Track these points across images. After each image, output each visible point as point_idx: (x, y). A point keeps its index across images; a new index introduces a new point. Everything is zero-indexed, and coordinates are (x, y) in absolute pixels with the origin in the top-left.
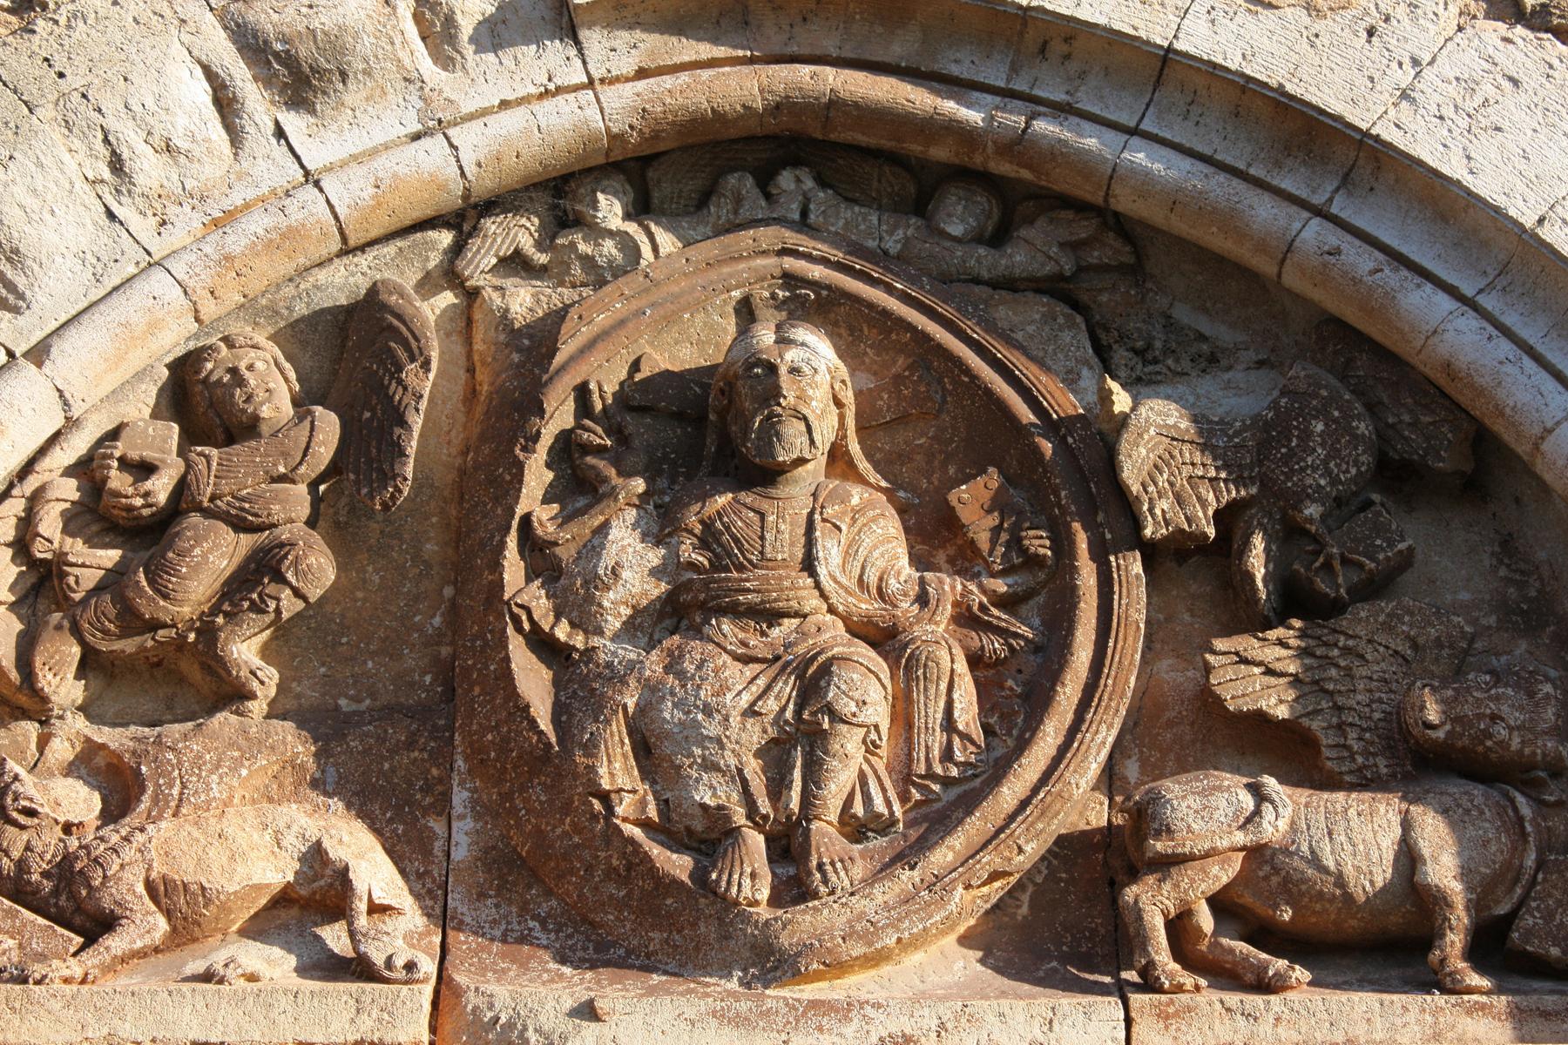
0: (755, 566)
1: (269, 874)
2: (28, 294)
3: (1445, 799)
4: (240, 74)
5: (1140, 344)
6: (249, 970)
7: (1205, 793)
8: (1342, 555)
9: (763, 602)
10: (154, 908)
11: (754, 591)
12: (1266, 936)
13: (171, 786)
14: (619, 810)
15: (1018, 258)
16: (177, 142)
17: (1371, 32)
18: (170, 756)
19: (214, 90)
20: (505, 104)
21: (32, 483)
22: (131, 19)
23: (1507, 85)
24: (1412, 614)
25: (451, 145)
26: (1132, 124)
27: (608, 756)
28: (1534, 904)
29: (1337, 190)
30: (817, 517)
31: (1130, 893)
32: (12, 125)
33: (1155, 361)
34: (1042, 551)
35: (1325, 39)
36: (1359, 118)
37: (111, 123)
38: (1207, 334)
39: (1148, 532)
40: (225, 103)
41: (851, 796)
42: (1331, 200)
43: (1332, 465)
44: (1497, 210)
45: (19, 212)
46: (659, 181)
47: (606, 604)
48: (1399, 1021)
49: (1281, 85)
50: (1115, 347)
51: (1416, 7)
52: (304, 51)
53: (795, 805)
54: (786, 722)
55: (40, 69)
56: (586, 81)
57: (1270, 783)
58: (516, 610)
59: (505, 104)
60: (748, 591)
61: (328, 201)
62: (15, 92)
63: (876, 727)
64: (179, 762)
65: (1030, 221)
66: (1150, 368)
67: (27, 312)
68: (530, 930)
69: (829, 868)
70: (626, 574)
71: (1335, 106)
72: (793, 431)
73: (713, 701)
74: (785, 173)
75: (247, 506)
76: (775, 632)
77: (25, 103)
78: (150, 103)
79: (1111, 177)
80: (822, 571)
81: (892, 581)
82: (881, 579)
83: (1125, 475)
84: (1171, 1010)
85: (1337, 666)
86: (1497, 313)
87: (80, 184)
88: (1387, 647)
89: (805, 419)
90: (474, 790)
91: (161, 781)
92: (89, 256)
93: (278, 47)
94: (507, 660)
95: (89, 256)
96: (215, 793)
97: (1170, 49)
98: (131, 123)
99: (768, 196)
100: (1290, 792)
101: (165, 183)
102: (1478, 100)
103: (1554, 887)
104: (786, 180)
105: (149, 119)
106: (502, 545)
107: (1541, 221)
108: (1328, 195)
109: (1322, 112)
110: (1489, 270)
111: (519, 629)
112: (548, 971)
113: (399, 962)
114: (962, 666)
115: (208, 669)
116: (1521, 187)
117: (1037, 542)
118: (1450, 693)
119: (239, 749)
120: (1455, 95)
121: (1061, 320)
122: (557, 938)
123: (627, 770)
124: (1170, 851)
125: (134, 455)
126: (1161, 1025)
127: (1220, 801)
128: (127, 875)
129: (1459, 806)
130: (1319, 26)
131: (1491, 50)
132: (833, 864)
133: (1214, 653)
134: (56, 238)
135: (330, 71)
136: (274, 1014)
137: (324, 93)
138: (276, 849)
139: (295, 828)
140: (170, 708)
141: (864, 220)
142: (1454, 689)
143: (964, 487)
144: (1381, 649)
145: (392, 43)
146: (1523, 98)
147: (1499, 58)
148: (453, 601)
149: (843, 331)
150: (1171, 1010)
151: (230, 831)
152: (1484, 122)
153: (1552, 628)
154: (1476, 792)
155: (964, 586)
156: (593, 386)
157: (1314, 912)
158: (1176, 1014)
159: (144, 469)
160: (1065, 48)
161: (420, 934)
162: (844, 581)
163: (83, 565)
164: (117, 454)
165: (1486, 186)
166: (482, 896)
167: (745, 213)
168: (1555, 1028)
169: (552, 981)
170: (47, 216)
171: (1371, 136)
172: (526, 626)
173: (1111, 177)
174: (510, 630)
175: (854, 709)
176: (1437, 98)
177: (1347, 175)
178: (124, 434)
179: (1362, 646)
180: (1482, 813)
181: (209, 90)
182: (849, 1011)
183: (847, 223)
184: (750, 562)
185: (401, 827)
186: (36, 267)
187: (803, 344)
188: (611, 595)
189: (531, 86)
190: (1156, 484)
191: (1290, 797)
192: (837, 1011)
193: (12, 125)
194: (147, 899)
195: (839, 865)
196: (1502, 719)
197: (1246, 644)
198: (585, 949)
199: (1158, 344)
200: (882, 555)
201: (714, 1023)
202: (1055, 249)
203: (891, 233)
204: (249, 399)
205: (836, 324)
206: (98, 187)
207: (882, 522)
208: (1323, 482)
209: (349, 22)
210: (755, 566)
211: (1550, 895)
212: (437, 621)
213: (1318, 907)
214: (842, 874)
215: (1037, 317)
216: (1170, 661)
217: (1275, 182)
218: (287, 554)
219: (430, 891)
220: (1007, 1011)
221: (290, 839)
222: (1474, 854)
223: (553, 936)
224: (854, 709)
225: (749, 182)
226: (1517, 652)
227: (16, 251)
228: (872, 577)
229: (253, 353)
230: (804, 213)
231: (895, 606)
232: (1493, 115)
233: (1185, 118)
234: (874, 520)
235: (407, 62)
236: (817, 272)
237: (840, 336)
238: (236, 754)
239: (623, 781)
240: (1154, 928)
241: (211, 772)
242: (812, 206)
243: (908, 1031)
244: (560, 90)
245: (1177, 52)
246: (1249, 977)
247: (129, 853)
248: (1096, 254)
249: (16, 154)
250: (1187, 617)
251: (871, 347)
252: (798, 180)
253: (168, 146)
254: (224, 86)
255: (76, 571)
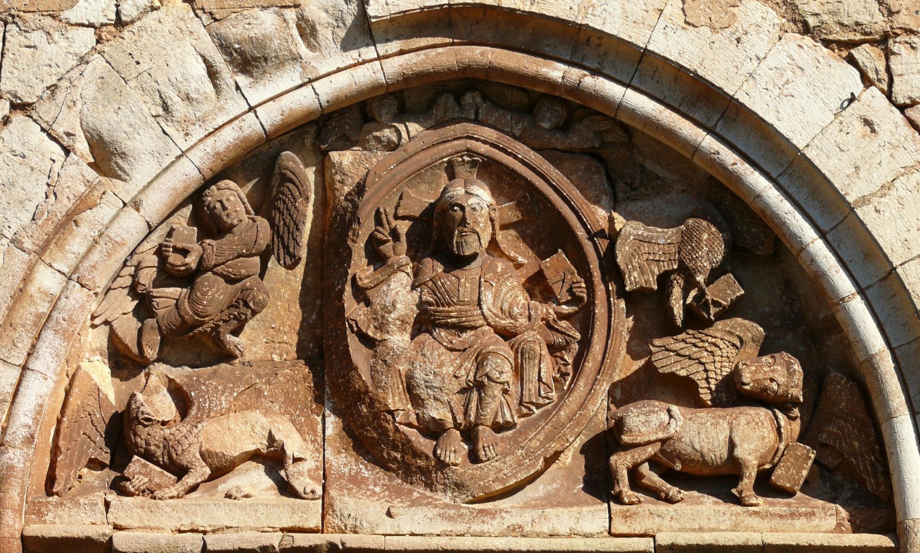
0: (455, 304)
1: (250, 446)
2: (130, 173)
3: (749, 417)
4: (219, 60)
5: (629, 181)
6: (246, 493)
7: (647, 414)
8: (713, 300)
9: (458, 323)
10: (204, 464)
11: (455, 317)
12: (669, 475)
13: (205, 403)
14: (397, 419)
15: (574, 140)
16: (193, 95)
17: (738, 40)
18: (203, 388)
19: (207, 67)
20: (339, 70)
21: (136, 258)
22: (168, 32)
23: (798, 71)
24: (741, 327)
25: (316, 93)
26: (628, 82)
27: (393, 394)
28: (782, 464)
29: (719, 120)
30: (482, 280)
31: (613, 459)
32: (118, 91)
33: (636, 189)
34: (581, 294)
35: (716, 45)
36: (730, 90)
37: (163, 89)
38: (660, 175)
39: (627, 289)
40: (213, 74)
41: (497, 413)
42: (716, 125)
43: (710, 255)
44: (788, 140)
45: (124, 135)
46: (409, 96)
47: (390, 320)
48: (721, 519)
49: (696, 71)
50: (618, 180)
51: (760, 27)
52: (247, 48)
53: (472, 418)
54: (469, 381)
55: (128, 60)
56: (376, 56)
57: (675, 409)
58: (351, 322)
59: (339, 70)
60: (452, 317)
61: (261, 123)
62: (118, 72)
63: (508, 383)
64: (208, 391)
65: (581, 120)
66: (633, 193)
67: (130, 182)
68: (361, 469)
69: (487, 449)
70: (398, 306)
71: (719, 82)
72: (472, 238)
73: (437, 370)
74: (468, 95)
75: (231, 270)
76: (464, 335)
77: (123, 78)
78: (179, 77)
79: (617, 109)
80: (485, 307)
81: (515, 309)
82: (510, 308)
83: (618, 260)
84: (628, 514)
85: (707, 350)
86: (786, 187)
87: (151, 119)
88: (729, 342)
89: (478, 234)
90: (334, 403)
91: (201, 400)
92: (156, 153)
93: (237, 46)
94: (347, 346)
95: (156, 153)
96: (224, 405)
97: (645, 49)
98: (171, 88)
99: (459, 104)
100: (683, 411)
101: (187, 115)
102: (785, 80)
103: (791, 457)
104: (468, 98)
105: (180, 85)
106: (342, 291)
107: (807, 146)
108: (715, 122)
109: (713, 85)
110: (784, 164)
111: (353, 331)
112: (369, 490)
113: (308, 490)
114: (545, 352)
115: (215, 343)
116: (800, 128)
117: (579, 290)
118: (754, 368)
119: (232, 383)
120: (773, 76)
121: (593, 169)
122: (372, 474)
123: (400, 400)
124: (631, 442)
125: (179, 245)
126: (624, 521)
127: (653, 417)
128: (192, 449)
129: (753, 421)
130: (715, 37)
131: (792, 53)
132: (488, 447)
133: (653, 346)
134: (141, 146)
135: (260, 58)
136: (259, 514)
137: (257, 67)
138: (252, 434)
139: (259, 423)
140: (199, 358)
141: (504, 118)
142: (756, 366)
143: (548, 260)
144: (727, 343)
145: (288, 42)
146: (804, 80)
147: (796, 57)
148: (321, 307)
149: (494, 177)
150: (628, 514)
151: (232, 426)
152: (786, 92)
153: (803, 327)
154: (761, 413)
155: (547, 310)
156: (382, 210)
157: (691, 467)
158: (630, 516)
159: (185, 252)
160: (598, 41)
161: (314, 470)
162: (495, 311)
163: (160, 297)
164: (172, 245)
165: (782, 127)
166: (339, 452)
167: (449, 115)
168: (785, 522)
169: (371, 496)
170: (137, 136)
171: (734, 99)
172: (355, 329)
173: (617, 109)
174: (348, 332)
175: (498, 376)
176: (767, 79)
177: (724, 113)
178: (174, 233)
179: (719, 342)
180: (763, 424)
181: (205, 67)
182: (495, 514)
183: (496, 119)
184: (453, 302)
185: (303, 419)
186: (133, 161)
187: (477, 196)
188: (392, 315)
189: (351, 59)
190: (632, 264)
191: (683, 415)
192: (490, 514)
193: (118, 91)
194: (201, 460)
195: (491, 447)
196: (775, 381)
197: (668, 341)
198: (384, 479)
199: (637, 181)
200: (511, 296)
201: (439, 519)
202: (591, 135)
203: (517, 124)
204: (228, 215)
205: (491, 173)
206: (157, 118)
207: (511, 280)
208: (705, 264)
209: (267, 32)
210: (455, 304)
211: (789, 460)
212: (314, 316)
213: (692, 465)
214: (493, 452)
215: (583, 167)
216: (636, 342)
217: (691, 115)
218: (249, 294)
219: (317, 449)
220: (560, 514)
221: (258, 429)
222: (758, 443)
223: (370, 472)
224: (498, 376)
225: (451, 99)
226: (788, 338)
227: (124, 153)
228: (506, 307)
229: (228, 192)
230: (477, 114)
231: (516, 321)
232: (790, 89)
233: (652, 79)
234: (507, 279)
235: (294, 51)
236: (483, 148)
237: (493, 179)
238: (231, 385)
239: (399, 406)
240: (623, 476)
241: (222, 395)
242: (480, 111)
243: (519, 523)
244: (364, 62)
245: (649, 51)
246: (663, 495)
247: (192, 439)
248: (610, 136)
249: (121, 107)
250: (644, 319)
251: (507, 185)
252: (474, 98)
253: (188, 97)
254: (212, 66)
255: (157, 300)
